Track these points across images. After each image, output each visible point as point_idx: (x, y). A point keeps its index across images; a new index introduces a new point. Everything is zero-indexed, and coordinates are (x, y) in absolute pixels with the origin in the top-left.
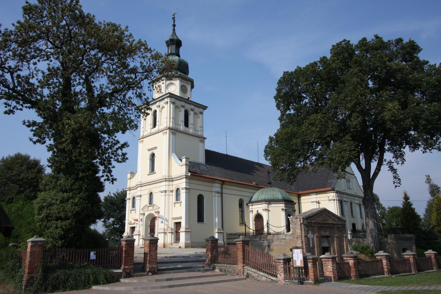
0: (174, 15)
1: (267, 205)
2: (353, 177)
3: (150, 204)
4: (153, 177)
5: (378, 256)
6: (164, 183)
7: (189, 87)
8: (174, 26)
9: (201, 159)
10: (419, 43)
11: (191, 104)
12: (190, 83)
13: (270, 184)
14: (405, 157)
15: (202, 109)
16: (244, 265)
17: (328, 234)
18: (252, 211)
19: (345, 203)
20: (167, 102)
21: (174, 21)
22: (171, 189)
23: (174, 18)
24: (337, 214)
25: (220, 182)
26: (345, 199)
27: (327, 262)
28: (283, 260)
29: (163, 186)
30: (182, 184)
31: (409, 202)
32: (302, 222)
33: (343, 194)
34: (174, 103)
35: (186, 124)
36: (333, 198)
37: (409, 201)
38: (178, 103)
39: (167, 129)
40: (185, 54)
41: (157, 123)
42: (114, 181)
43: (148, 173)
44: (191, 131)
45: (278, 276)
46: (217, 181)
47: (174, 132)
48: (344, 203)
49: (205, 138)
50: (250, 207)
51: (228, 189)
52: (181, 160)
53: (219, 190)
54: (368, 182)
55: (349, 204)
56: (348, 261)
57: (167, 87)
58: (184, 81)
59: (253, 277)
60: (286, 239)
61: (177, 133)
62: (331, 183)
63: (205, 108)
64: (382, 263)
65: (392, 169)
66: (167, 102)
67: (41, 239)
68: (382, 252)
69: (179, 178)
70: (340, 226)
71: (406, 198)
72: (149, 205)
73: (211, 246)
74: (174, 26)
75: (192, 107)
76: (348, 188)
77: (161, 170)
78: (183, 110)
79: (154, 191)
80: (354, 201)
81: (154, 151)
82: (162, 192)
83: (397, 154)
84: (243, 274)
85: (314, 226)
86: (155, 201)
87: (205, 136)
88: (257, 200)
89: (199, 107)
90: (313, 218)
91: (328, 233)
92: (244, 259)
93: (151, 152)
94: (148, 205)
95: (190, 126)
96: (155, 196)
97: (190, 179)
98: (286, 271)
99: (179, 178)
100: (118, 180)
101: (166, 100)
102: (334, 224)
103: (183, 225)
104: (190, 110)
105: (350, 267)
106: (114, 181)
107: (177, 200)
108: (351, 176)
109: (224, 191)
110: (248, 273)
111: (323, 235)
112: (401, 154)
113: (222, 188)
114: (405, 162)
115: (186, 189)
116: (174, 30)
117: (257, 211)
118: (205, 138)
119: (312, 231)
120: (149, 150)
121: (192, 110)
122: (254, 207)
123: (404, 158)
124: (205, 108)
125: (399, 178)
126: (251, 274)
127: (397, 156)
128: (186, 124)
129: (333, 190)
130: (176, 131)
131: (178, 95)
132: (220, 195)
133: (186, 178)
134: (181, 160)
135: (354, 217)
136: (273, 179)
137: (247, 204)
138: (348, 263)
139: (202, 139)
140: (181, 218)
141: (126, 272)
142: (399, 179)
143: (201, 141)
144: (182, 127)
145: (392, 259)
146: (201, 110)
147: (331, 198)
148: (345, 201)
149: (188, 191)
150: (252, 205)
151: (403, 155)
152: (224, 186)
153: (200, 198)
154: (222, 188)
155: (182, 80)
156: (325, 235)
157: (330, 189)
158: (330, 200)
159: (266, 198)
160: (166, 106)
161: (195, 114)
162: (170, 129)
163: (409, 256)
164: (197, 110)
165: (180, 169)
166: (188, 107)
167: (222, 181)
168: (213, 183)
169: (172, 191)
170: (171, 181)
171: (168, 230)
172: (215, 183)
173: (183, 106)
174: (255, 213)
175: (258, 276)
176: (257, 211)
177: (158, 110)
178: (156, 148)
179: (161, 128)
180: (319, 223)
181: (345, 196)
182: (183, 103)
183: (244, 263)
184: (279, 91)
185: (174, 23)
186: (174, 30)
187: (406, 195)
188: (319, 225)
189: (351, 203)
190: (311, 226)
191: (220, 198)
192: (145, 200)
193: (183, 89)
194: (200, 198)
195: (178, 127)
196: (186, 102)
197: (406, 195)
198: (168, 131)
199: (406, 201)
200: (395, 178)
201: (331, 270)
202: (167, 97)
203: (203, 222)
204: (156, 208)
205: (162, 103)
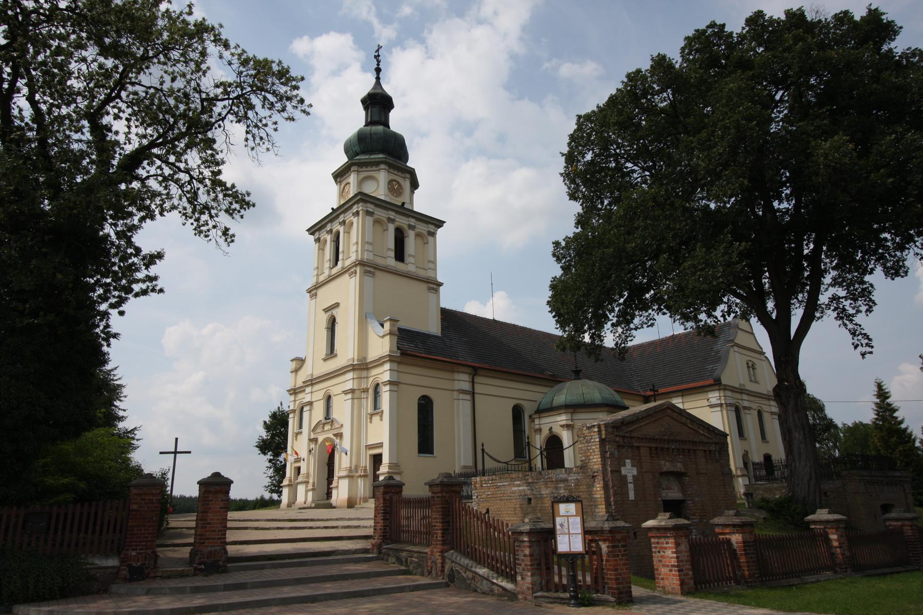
0: (378, 51)
1: (569, 416)
2: (763, 358)
3: (326, 419)
4: (333, 365)
5: (814, 522)
6: (350, 375)
7: (407, 185)
8: (378, 70)
9: (433, 327)
10: (890, 14)
11: (408, 216)
12: (408, 176)
13: (577, 374)
14: (875, 296)
15: (433, 227)
16: (446, 547)
17: (679, 467)
18: (540, 430)
19: (747, 411)
20: (358, 213)
21: (379, 62)
22: (364, 386)
23: (379, 56)
24: (721, 429)
25: (469, 370)
26: (746, 404)
27: (662, 540)
28: (529, 533)
29: (348, 381)
30: (384, 374)
31: (889, 405)
32: (603, 437)
33: (741, 391)
34: (369, 213)
35: (400, 255)
36: (719, 402)
37: (888, 401)
38: (381, 214)
39: (356, 265)
40: (397, 121)
41: (341, 257)
42: (112, 340)
43: (323, 356)
44: (409, 266)
45: (519, 578)
46: (461, 369)
47: (372, 270)
48: (742, 412)
49: (440, 284)
50: (537, 421)
51: (487, 386)
52: (382, 326)
53: (467, 386)
54: (787, 350)
55: (756, 412)
56: (727, 536)
57: (360, 183)
58: (396, 172)
59: (464, 580)
60: (567, 480)
61: (378, 273)
62: (713, 371)
63: (439, 224)
64: (828, 541)
65: (843, 316)
66: (358, 213)
67: (686, 522)
68: (826, 511)
69: (379, 362)
70: (713, 448)
71: (882, 394)
72: (324, 421)
73: (384, 499)
74: (378, 70)
75: (412, 222)
76: (751, 381)
77: (347, 352)
78: (391, 228)
79: (335, 391)
80: (765, 408)
81: (335, 312)
82: (345, 392)
83: (856, 290)
84: (443, 571)
85: (638, 448)
86: (335, 415)
87: (440, 280)
88: (549, 406)
89: (427, 223)
90: (636, 426)
91: (679, 465)
92: (445, 531)
93: (330, 313)
94: (324, 421)
95: (408, 259)
96: (335, 401)
97: (399, 363)
98: (539, 564)
99: (379, 362)
100: (121, 338)
101: (355, 209)
102: (694, 443)
103: (386, 459)
104: (406, 227)
105: (733, 553)
106: (112, 340)
107: (375, 408)
108: (757, 356)
109: (478, 388)
110: (452, 570)
111: (665, 469)
112: (864, 290)
113: (473, 383)
114: (874, 308)
115: (390, 383)
116: (378, 78)
117: (551, 429)
118: (440, 284)
119: (633, 459)
120: (326, 310)
121: (411, 227)
122: (544, 420)
123: (873, 298)
124: (439, 224)
125: (863, 332)
126: (459, 573)
127: (854, 294)
128: (400, 255)
129: (717, 384)
130: (375, 268)
131: (383, 198)
132: (468, 397)
133: (390, 361)
134: (382, 326)
135: (768, 442)
136: (558, 347)
137: (530, 416)
138: (729, 542)
139: (434, 286)
140: (380, 445)
141: (129, 566)
142: (866, 336)
143: (429, 289)
144: (391, 262)
145: (892, 274)
146: (431, 228)
147: (714, 401)
148: (745, 408)
149: (395, 388)
150: (540, 418)
151: (870, 293)
152: (477, 379)
153: (425, 407)
154: (473, 383)
155: (392, 170)
156: (672, 469)
157: (711, 381)
158: (711, 406)
159: (568, 402)
160: (355, 220)
161: (418, 235)
162: (361, 263)
163: (899, 523)
164: (422, 228)
165: (380, 344)
166: (402, 221)
167: (473, 367)
168: (453, 371)
169: (366, 391)
170: (364, 369)
171: (357, 472)
172: (459, 372)
173: (391, 220)
174: (545, 432)
175: (473, 578)
176: (551, 429)
177: (341, 229)
178: (337, 305)
179: (348, 263)
180: (653, 440)
181: (745, 397)
182: (392, 215)
183: (444, 542)
184: (570, 158)
185: (378, 65)
186: (378, 78)
187: (879, 386)
188: (654, 445)
189: (760, 414)
190: (632, 447)
191: (468, 404)
192: (318, 413)
193: (394, 188)
194: (425, 407)
195: (379, 261)
196: (397, 212)
197: (879, 386)
198: (358, 269)
199: (883, 401)
200: (854, 333)
201: (674, 562)
202: (357, 202)
203: (432, 453)
204: (337, 426)
205: (349, 217)
